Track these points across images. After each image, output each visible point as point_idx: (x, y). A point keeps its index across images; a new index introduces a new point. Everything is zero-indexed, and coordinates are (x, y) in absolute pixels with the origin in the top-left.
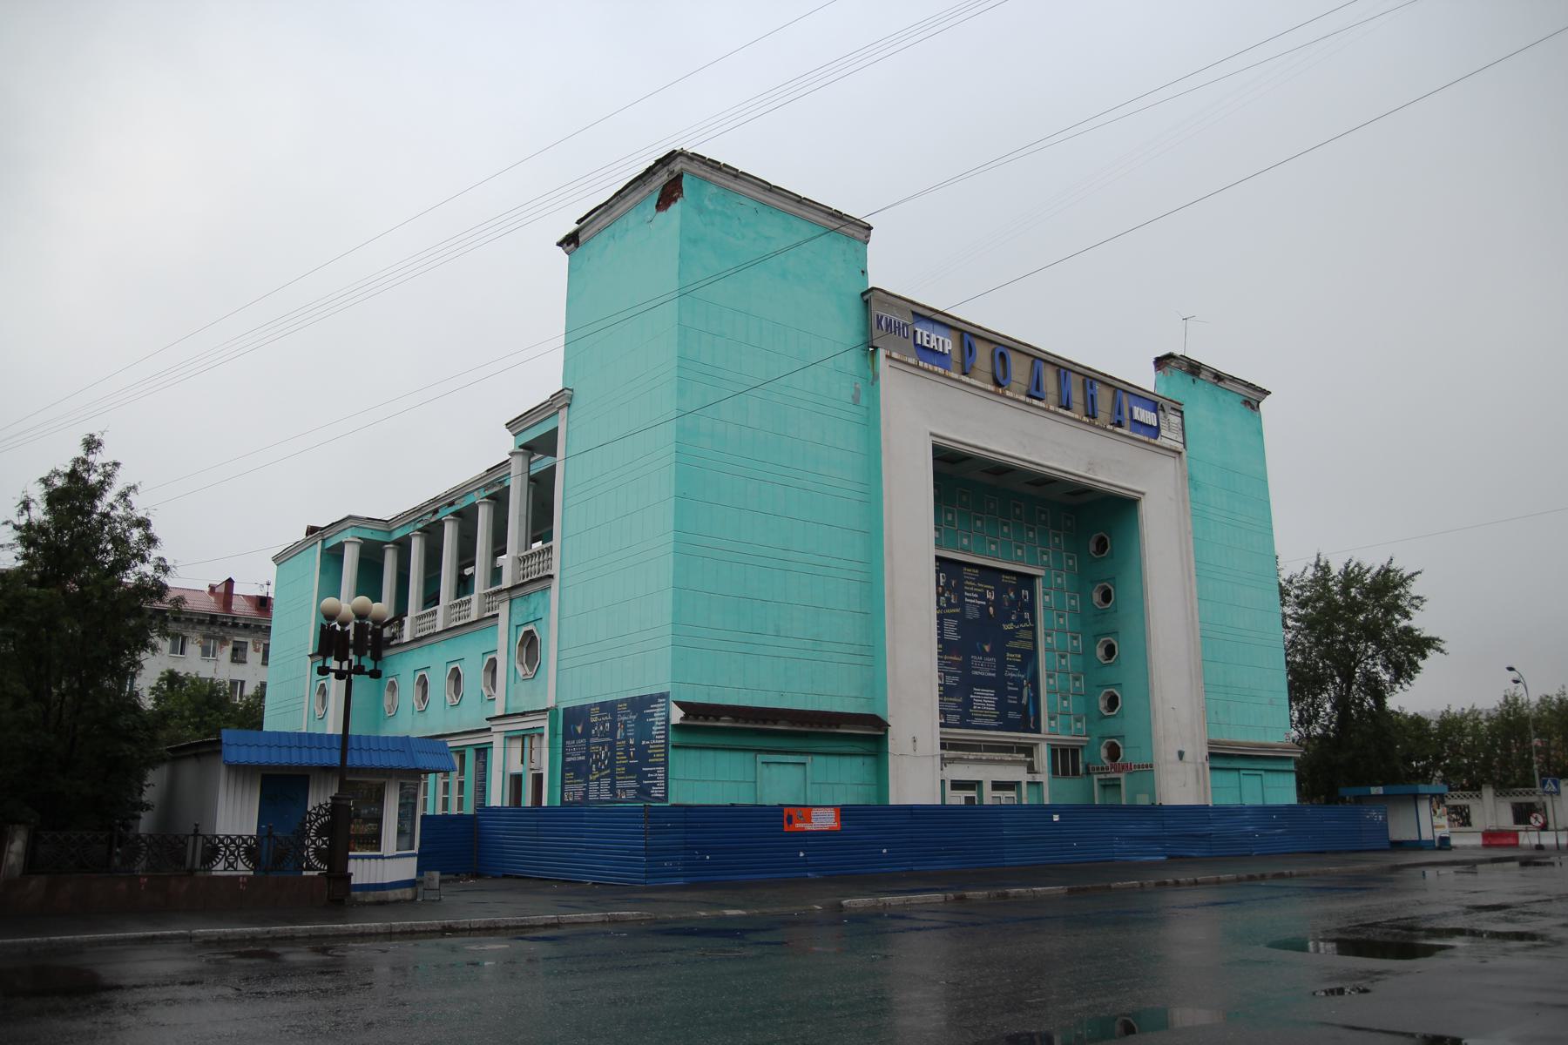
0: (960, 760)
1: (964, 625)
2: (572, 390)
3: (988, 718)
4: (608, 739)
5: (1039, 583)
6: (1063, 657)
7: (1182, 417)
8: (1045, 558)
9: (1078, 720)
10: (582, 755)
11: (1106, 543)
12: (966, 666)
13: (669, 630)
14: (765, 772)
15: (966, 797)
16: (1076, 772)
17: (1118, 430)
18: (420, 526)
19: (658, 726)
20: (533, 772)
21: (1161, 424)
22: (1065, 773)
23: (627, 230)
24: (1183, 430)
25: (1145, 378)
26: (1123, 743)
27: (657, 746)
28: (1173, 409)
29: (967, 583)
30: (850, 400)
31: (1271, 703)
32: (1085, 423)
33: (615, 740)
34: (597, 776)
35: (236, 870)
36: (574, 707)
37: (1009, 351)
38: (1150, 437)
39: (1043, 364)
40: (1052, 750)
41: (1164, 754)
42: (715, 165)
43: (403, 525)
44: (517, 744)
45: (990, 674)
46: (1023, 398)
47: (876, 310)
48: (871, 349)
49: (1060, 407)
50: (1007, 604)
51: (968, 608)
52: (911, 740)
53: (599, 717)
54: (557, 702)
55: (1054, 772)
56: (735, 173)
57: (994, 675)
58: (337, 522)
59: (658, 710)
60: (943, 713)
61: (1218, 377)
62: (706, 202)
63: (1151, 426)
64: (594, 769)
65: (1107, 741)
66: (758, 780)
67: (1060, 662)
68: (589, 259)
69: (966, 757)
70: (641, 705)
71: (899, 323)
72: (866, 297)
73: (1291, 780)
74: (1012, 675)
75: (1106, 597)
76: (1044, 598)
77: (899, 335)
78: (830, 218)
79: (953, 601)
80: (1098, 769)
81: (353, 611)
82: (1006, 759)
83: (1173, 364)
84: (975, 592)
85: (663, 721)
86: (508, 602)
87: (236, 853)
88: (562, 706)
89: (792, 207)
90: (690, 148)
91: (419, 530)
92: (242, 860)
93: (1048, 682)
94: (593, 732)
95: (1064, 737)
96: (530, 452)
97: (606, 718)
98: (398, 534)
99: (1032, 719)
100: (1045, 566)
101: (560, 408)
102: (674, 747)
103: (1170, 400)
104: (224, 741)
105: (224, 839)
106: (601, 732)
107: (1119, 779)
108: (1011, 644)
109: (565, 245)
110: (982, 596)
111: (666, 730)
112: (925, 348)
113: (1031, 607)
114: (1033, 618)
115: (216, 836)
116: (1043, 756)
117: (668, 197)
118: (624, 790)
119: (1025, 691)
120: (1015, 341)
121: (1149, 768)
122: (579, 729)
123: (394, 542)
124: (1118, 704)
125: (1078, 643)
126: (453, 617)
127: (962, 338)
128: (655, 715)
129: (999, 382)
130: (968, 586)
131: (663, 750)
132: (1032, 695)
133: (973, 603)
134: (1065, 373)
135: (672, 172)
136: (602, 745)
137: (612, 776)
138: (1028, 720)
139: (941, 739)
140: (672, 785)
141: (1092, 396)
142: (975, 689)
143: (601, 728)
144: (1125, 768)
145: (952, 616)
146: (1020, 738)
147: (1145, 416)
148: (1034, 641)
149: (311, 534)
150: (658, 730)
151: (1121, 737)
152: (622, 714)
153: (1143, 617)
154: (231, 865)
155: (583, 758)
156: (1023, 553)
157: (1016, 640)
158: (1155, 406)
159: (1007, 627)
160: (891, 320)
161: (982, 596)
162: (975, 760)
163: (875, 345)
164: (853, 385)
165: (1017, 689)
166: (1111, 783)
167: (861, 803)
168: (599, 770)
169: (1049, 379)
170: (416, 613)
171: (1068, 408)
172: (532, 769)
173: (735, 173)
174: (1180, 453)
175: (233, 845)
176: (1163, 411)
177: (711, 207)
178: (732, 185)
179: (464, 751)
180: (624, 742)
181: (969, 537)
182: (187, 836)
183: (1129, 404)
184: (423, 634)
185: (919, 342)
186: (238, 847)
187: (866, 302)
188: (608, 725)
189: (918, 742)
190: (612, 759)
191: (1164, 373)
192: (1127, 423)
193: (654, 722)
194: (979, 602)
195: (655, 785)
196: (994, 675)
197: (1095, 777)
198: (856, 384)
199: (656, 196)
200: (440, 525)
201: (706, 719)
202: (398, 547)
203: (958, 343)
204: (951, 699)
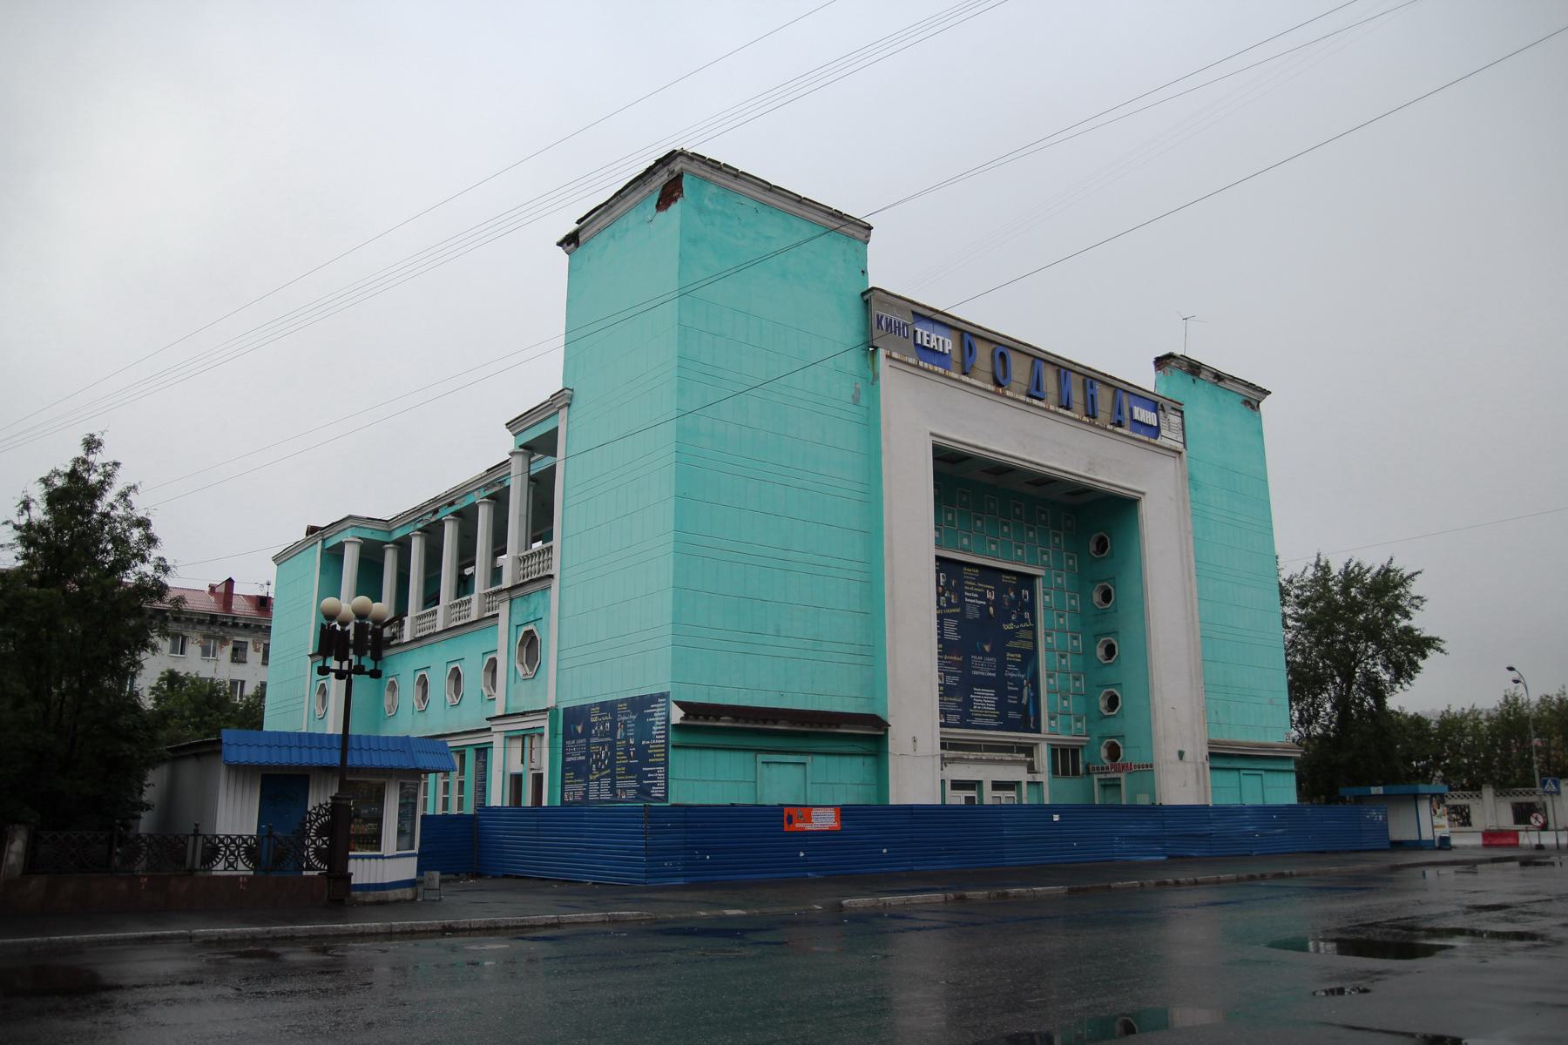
0: (960, 760)
1: (964, 625)
2: (572, 390)
4: (608, 739)
5: (1039, 583)
6: (1063, 657)
7: (1182, 417)
8: (1045, 557)
10: (582, 755)
11: (1106, 543)
12: (966, 666)
15: (966, 797)
16: (1076, 772)
17: (1119, 430)
18: (420, 526)
19: (658, 726)
21: (1161, 424)
22: (1065, 773)
23: (627, 230)
24: (1183, 429)
25: (1145, 378)
26: (1123, 743)
28: (1173, 409)
29: (967, 582)
30: (850, 400)
31: (1271, 703)
32: (1085, 423)
33: (615, 740)
35: (236, 870)
37: (1009, 351)
40: (1052, 749)
41: (1164, 754)
43: (404, 525)
44: (517, 744)
45: (990, 674)
46: (1023, 398)
47: (876, 310)
48: (871, 349)
50: (1007, 604)
51: (968, 607)
53: (599, 717)
54: (557, 702)
55: (1055, 771)
56: (735, 172)
57: (994, 675)
59: (658, 710)
60: (943, 713)
61: (1219, 377)
62: (706, 201)
63: (1152, 426)
65: (1107, 741)
67: (1060, 662)
68: (589, 259)
70: (641, 705)
71: (899, 323)
72: (866, 297)
73: (1291, 780)
74: (1012, 675)
75: (1107, 596)
76: (1044, 599)
79: (953, 601)
83: (1173, 364)
84: (975, 592)
86: (508, 602)
87: (236, 853)
88: (562, 706)
89: (793, 208)
91: (419, 530)
92: (242, 860)
93: (1048, 682)
94: (593, 732)
95: (1064, 737)
96: (530, 452)
97: (606, 718)
98: (398, 534)
100: (1045, 565)
102: (674, 747)
105: (224, 839)
106: (601, 732)
107: (1119, 779)
108: (1011, 644)
109: (565, 245)
110: (982, 596)
111: (667, 730)
112: (925, 348)
113: (1031, 607)
114: (1033, 618)
115: (217, 836)
116: (1043, 756)
117: (668, 197)
118: (624, 790)
119: (1026, 691)
122: (579, 729)
125: (1078, 643)
126: (454, 617)
127: (962, 337)
128: (655, 715)
129: (999, 382)
131: (663, 750)
134: (1091, 383)
135: (672, 172)
136: (602, 744)
137: (612, 775)
138: (1028, 719)
139: (941, 739)
140: (673, 785)
141: (1092, 396)
142: (975, 689)
143: (601, 728)
144: (1126, 767)
146: (1020, 738)
147: (1148, 417)
148: (1035, 640)
149: (311, 534)
150: (658, 730)
152: (622, 714)
153: (1143, 616)
155: (583, 758)
156: (1023, 553)
157: (1016, 640)
158: (1155, 406)
159: (1007, 627)
161: (982, 596)
166: (1111, 783)
167: (861, 803)
168: (599, 770)
171: (1068, 408)
172: (532, 769)
173: (735, 172)
174: (1180, 453)
176: (1163, 410)
177: (711, 207)
179: (464, 751)
181: (969, 537)
183: (1129, 402)
184: (423, 634)
186: (238, 847)
187: (867, 302)
188: (608, 725)
189: (918, 742)
190: (612, 758)
192: (1127, 423)
193: (654, 722)
195: (655, 785)
196: (994, 675)
198: (856, 384)
199: (656, 196)
200: (440, 524)
202: (398, 547)
204: (951, 699)
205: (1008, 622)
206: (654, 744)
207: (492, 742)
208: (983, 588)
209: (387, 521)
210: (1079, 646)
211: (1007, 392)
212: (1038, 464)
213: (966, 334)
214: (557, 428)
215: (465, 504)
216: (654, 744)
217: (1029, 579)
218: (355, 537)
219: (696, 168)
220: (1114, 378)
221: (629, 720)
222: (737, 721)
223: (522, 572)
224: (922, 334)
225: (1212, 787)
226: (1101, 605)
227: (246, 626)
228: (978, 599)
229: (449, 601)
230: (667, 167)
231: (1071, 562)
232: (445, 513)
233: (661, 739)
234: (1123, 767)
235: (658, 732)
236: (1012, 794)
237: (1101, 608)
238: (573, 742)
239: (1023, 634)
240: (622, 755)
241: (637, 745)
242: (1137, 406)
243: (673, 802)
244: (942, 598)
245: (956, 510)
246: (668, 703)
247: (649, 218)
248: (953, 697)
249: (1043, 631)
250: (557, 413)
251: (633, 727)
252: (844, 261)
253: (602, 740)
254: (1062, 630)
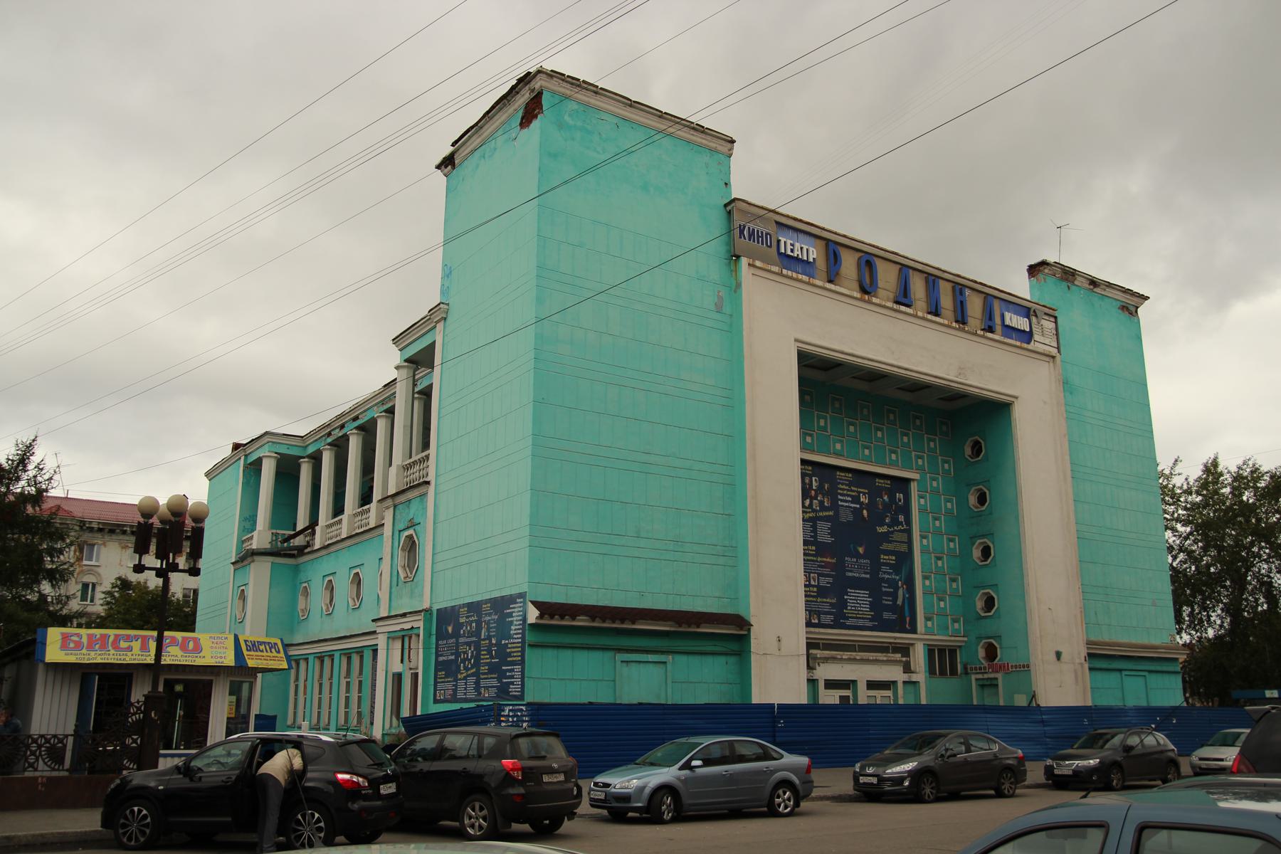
0: (834, 659)
1: (837, 528)
2: (448, 304)
3: (863, 618)
4: (474, 639)
5: (914, 487)
6: (939, 558)
7: (1056, 322)
8: (920, 462)
9: (955, 621)
10: (452, 654)
11: (981, 447)
12: (840, 568)
13: (527, 531)
14: (625, 670)
15: (840, 696)
16: (954, 672)
17: (989, 335)
18: (329, 440)
19: (516, 625)
20: (412, 671)
21: (1034, 329)
22: (943, 673)
23: (495, 149)
24: (1057, 335)
25: (1021, 287)
26: (1000, 644)
27: (515, 645)
28: (1046, 314)
29: (840, 486)
30: (713, 307)
31: (1154, 605)
32: (955, 328)
33: (480, 640)
34: (464, 675)
35: (36, 770)
36: (446, 608)
37: (839, 247)
38: (1022, 341)
39: (911, 271)
40: (929, 650)
41: (1040, 656)
42: (574, 81)
43: (316, 440)
44: (398, 645)
45: (863, 576)
46: (890, 304)
47: (738, 220)
48: (734, 258)
49: (929, 313)
50: (880, 507)
51: (841, 511)
52: (775, 639)
53: (467, 617)
54: (431, 603)
55: (931, 671)
56: (595, 89)
57: (868, 576)
58: (256, 439)
59: (516, 610)
60: (810, 611)
61: (1094, 283)
62: (567, 118)
63: (1024, 331)
64: (462, 669)
65: (984, 641)
66: (617, 678)
67: (936, 563)
68: (463, 180)
69: (839, 657)
70: (502, 604)
71: (762, 233)
72: (729, 208)
73: (1177, 682)
74: (887, 576)
75: (982, 499)
76: (919, 502)
77: (762, 244)
78: (692, 132)
79: (826, 504)
80: (980, 669)
81: (168, 509)
82: (881, 658)
83: (1046, 271)
84: (848, 496)
85: (520, 620)
86: (392, 509)
87: (38, 753)
88: (435, 607)
89: (684, 133)
90: (548, 66)
91: (329, 444)
92: (43, 760)
93: (924, 584)
94: (462, 632)
95: (941, 638)
96: (415, 366)
97: (473, 618)
98: (311, 450)
99: (908, 619)
100: (920, 469)
101: (437, 322)
102: (531, 646)
103: (1044, 306)
104: (38, 641)
105: (38, 739)
106: (469, 631)
107: (996, 679)
108: (885, 546)
109: (443, 167)
110: (856, 499)
111: (523, 629)
112: (789, 256)
113: (906, 510)
114: (908, 521)
115: (30, 736)
116: (919, 656)
117: (531, 113)
118: (487, 688)
119: (900, 592)
120: (882, 249)
121: (1026, 668)
122: (450, 629)
123: (309, 456)
124: (994, 605)
125: (955, 545)
126: (356, 525)
127: (827, 245)
128: (514, 614)
129: (867, 289)
130: (841, 489)
131: (520, 649)
132: (907, 596)
133: (846, 506)
134: (934, 281)
135: (533, 91)
136: (469, 644)
137: (477, 674)
138: (905, 621)
139: (807, 638)
140: (529, 684)
141: (962, 302)
142: (849, 590)
143: (469, 628)
144: (1003, 668)
145: (826, 519)
146: (895, 638)
147: (1021, 323)
148: (910, 543)
149: (236, 450)
150: (515, 630)
151: (998, 637)
152: (486, 614)
153: (1017, 518)
154: (31, 765)
155: (453, 657)
156: (897, 457)
157: (891, 542)
158: (1027, 311)
159: (881, 530)
160: (753, 230)
161: (856, 499)
162: (849, 659)
163: (737, 253)
164: (717, 293)
165: (892, 590)
166: (989, 683)
167: (723, 701)
168: (466, 669)
169: (918, 288)
170: (326, 521)
171: (937, 314)
172: (411, 669)
173: (595, 89)
174: (1053, 357)
175: (34, 745)
176: (1036, 316)
177: (571, 122)
178: (593, 101)
179: (363, 652)
180: (487, 642)
181: (841, 442)
182: (67, 736)
183: (1001, 310)
184: (330, 542)
185: (783, 251)
186: (40, 747)
187: (729, 213)
188: (474, 625)
189: (783, 641)
190: (477, 657)
191: (1037, 280)
192: (998, 328)
193: (512, 622)
194: (853, 505)
195: (512, 683)
196: (868, 576)
197: (973, 677)
198: (719, 292)
199: (520, 114)
200: (346, 438)
201: (562, 618)
202: (313, 461)
203: (823, 252)
204: (825, 600)
205: (882, 525)
206: (511, 643)
207: (377, 645)
208: (857, 492)
209: (302, 437)
210: (955, 548)
211: (873, 298)
212: (906, 369)
213: (830, 243)
214: (434, 342)
215: (366, 419)
216: (511, 643)
217: (902, 484)
218: (272, 452)
219: (555, 85)
220: (985, 285)
221: (492, 620)
222: (680, 626)
223: (405, 479)
224: (785, 242)
225: (1091, 688)
226: (977, 508)
227: (100, 530)
228: (852, 502)
229: (353, 510)
230: (528, 86)
231: (946, 466)
232: (350, 429)
233: (518, 638)
234: (1000, 667)
235: (515, 632)
236: (888, 693)
237: (976, 510)
238: (445, 642)
239: (897, 536)
240: (485, 655)
241: (498, 644)
242: (1008, 312)
243: (529, 701)
244: (815, 501)
245: (885, 427)
246: (524, 603)
247: (514, 135)
248: (827, 598)
249: (919, 533)
250: (435, 327)
251: (494, 627)
252: (707, 173)
253: (469, 640)
254: (938, 533)
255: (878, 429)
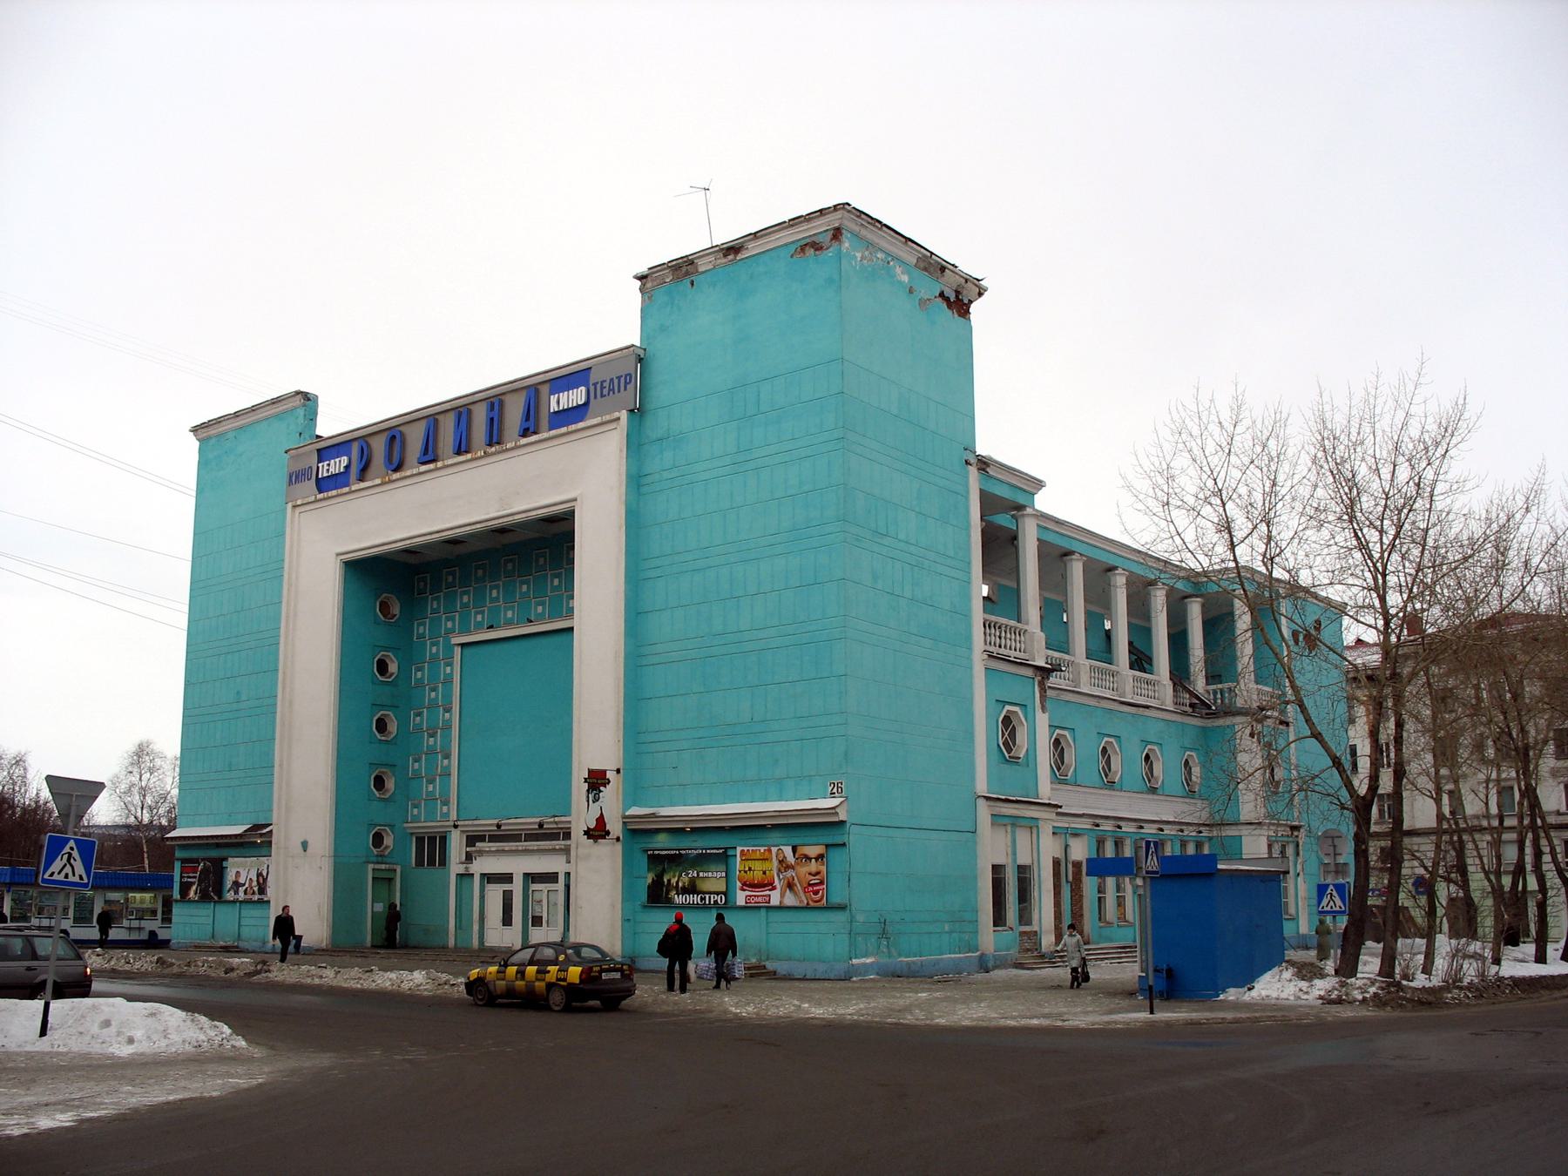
78: (274, 406)
212: (438, 532)
255: (523, 583)
